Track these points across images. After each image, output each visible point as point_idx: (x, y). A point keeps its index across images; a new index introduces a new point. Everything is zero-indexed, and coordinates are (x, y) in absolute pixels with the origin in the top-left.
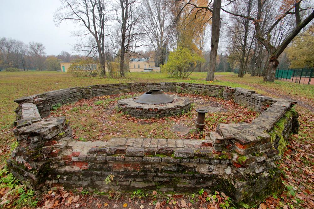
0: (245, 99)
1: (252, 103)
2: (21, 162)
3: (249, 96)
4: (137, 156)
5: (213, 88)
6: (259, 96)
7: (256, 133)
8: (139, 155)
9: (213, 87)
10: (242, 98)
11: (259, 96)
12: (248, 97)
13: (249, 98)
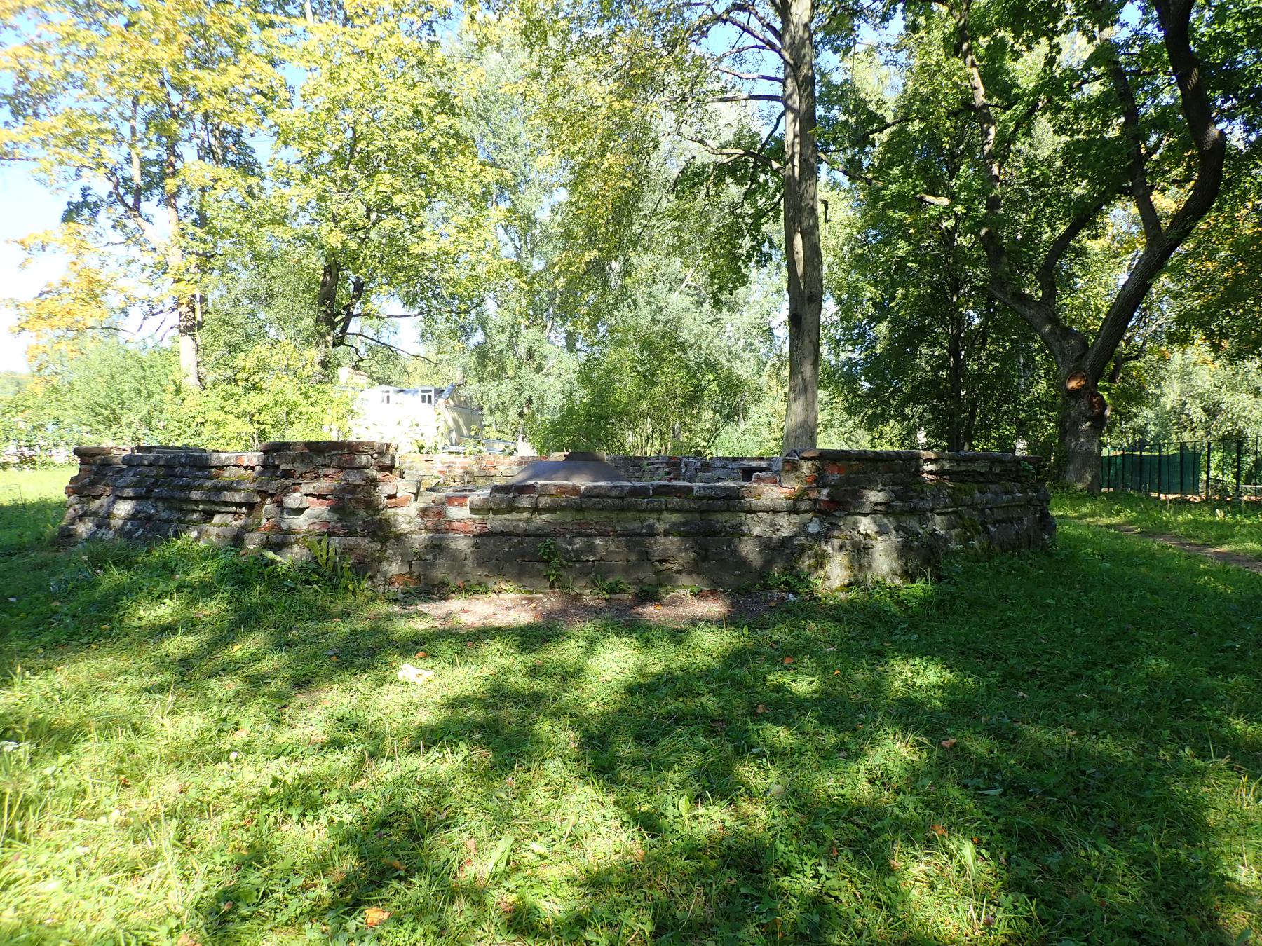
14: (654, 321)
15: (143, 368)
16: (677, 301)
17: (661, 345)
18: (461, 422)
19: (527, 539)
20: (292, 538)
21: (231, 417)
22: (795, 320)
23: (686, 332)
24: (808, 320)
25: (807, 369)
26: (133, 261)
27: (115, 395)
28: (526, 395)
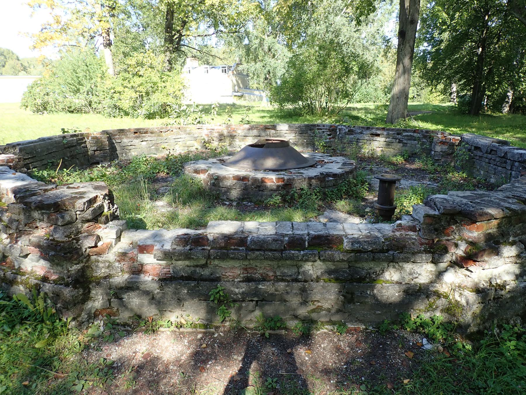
0: (483, 159)
1: (500, 168)
2: (473, 12)
3: (493, 152)
4: (271, 250)
5: (407, 136)
6: (516, 151)
7: (502, 203)
8: (274, 247)
9: (407, 134)
10: (478, 157)
11: (516, 151)
12: (490, 154)
13: (493, 157)
14: (327, 32)
15: (86, 65)
16: (339, 20)
17: (331, 47)
18: (240, 82)
19: (202, 283)
20: (19, 279)
21: (126, 89)
22: (402, 34)
23: (343, 36)
24: (409, 34)
25: (407, 61)
26: (79, 11)
27: (75, 79)
28: (267, 69)
